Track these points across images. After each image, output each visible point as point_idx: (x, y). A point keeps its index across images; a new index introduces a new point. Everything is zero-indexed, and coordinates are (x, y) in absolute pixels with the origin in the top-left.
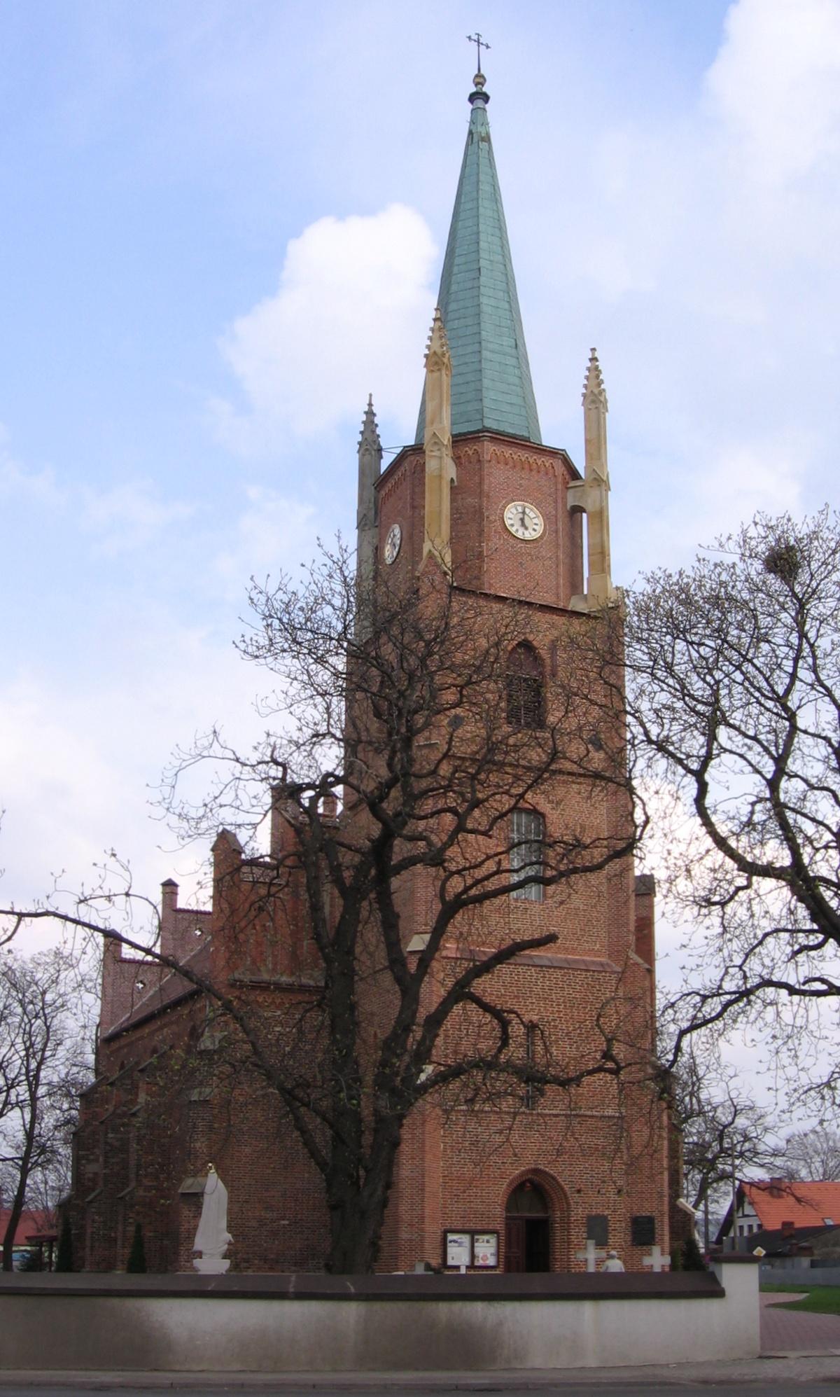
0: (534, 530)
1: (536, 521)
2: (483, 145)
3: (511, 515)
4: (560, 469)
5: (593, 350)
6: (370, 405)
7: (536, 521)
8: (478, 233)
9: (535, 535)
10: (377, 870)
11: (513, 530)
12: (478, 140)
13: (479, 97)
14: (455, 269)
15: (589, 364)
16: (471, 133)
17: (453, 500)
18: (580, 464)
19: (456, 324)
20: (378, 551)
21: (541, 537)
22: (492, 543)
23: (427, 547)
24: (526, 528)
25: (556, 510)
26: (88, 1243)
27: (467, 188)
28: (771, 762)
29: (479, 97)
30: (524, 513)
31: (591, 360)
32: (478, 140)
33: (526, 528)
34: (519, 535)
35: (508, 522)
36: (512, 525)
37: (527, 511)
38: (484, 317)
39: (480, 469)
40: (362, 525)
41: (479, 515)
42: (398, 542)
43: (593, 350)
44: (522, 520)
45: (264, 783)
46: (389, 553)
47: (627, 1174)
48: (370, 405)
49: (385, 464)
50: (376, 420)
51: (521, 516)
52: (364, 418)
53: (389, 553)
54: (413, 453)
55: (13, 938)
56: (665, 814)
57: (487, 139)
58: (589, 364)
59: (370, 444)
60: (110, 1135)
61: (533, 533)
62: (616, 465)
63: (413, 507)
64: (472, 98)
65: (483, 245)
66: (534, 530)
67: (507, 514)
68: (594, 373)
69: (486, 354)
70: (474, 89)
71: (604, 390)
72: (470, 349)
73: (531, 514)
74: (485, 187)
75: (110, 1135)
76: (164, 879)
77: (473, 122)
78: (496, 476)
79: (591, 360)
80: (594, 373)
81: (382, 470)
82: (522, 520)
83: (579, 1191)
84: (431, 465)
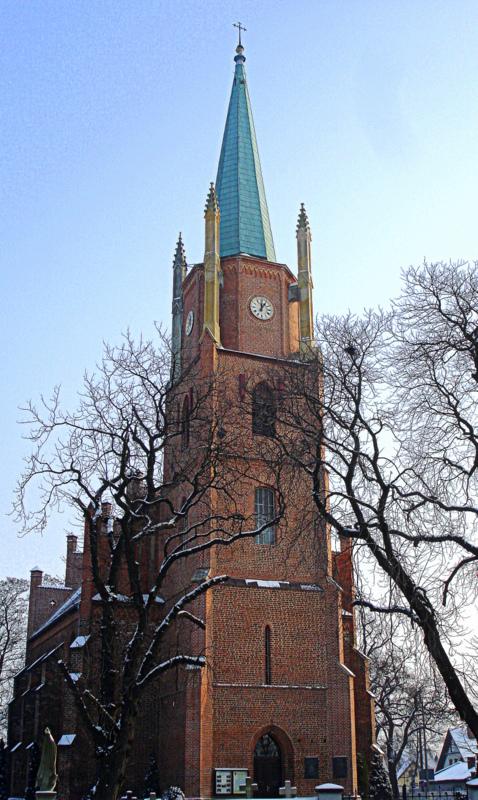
2: (242, 86)
3: (255, 305)
4: (284, 277)
5: (302, 204)
6: (180, 239)
12: (239, 82)
13: (239, 58)
14: (226, 158)
16: (235, 79)
17: (221, 297)
21: (272, 318)
22: (244, 323)
23: (205, 326)
25: (281, 300)
26: (12, 780)
27: (233, 111)
28: (345, 466)
29: (239, 58)
32: (239, 82)
35: (253, 309)
38: (241, 187)
39: (237, 277)
41: (235, 305)
46: (188, 328)
48: (180, 239)
52: (177, 246)
53: (188, 328)
55: (380, 448)
56: (229, 517)
57: (243, 82)
59: (179, 260)
62: (315, 275)
63: (200, 302)
64: (236, 59)
65: (241, 144)
68: (303, 220)
70: (237, 54)
72: (233, 206)
75: (28, 706)
77: (236, 73)
78: (246, 282)
80: (303, 220)
84: (207, 276)
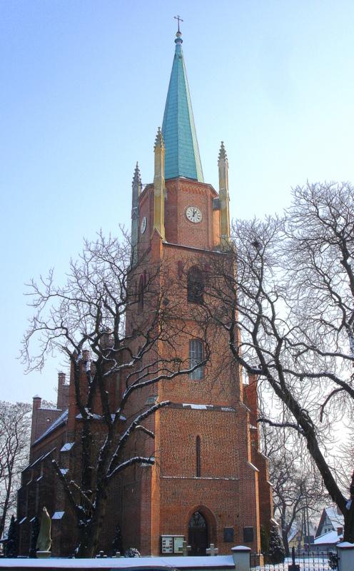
3: (189, 212)
4: (209, 193)
5: (222, 142)
6: (137, 166)
8: (177, 96)
10: (73, 448)
12: (178, 58)
13: (178, 41)
18: (217, 189)
19: (169, 133)
27: (173, 77)
29: (178, 41)
32: (178, 58)
40: (133, 217)
41: (175, 213)
48: (137, 166)
50: (140, 173)
52: (135, 172)
53: (143, 229)
54: (150, 186)
57: (181, 57)
59: (137, 181)
60: (31, 492)
62: (232, 192)
64: (176, 41)
69: (179, 145)
70: (176, 38)
71: (17, 403)
74: (180, 77)
75: (31, 492)
76: (33, 396)
77: (176, 51)
78: (183, 196)
83: (220, 516)
84: (156, 192)
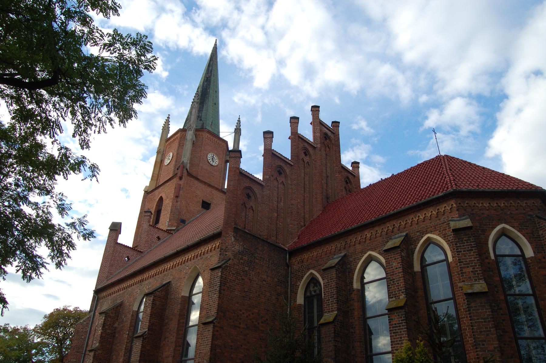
0: (216, 163)
1: (216, 160)
3: (210, 156)
6: (239, 118)
7: (216, 160)
9: (216, 165)
11: (209, 161)
15: (167, 119)
20: (162, 161)
21: (217, 166)
24: (213, 162)
30: (213, 156)
31: (168, 118)
33: (213, 162)
34: (211, 163)
36: (209, 160)
37: (214, 156)
42: (171, 158)
43: (169, 115)
44: (213, 159)
45: (70, 255)
47: (457, 210)
48: (239, 118)
49: (169, 135)
51: (212, 157)
58: (167, 119)
61: (215, 164)
66: (216, 163)
67: (209, 156)
68: (239, 121)
73: (216, 158)
79: (168, 118)
81: (168, 137)
82: (213, 159)
